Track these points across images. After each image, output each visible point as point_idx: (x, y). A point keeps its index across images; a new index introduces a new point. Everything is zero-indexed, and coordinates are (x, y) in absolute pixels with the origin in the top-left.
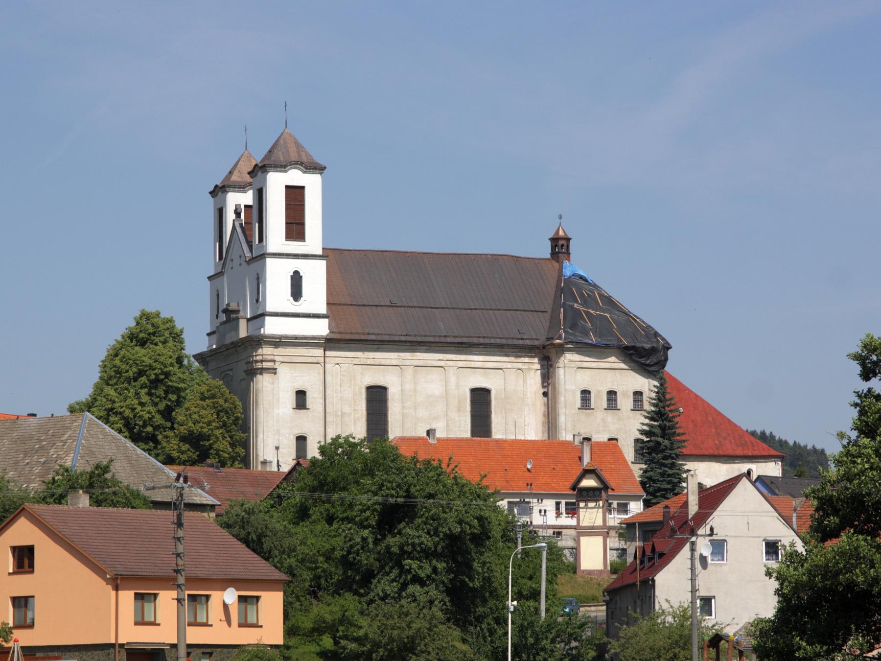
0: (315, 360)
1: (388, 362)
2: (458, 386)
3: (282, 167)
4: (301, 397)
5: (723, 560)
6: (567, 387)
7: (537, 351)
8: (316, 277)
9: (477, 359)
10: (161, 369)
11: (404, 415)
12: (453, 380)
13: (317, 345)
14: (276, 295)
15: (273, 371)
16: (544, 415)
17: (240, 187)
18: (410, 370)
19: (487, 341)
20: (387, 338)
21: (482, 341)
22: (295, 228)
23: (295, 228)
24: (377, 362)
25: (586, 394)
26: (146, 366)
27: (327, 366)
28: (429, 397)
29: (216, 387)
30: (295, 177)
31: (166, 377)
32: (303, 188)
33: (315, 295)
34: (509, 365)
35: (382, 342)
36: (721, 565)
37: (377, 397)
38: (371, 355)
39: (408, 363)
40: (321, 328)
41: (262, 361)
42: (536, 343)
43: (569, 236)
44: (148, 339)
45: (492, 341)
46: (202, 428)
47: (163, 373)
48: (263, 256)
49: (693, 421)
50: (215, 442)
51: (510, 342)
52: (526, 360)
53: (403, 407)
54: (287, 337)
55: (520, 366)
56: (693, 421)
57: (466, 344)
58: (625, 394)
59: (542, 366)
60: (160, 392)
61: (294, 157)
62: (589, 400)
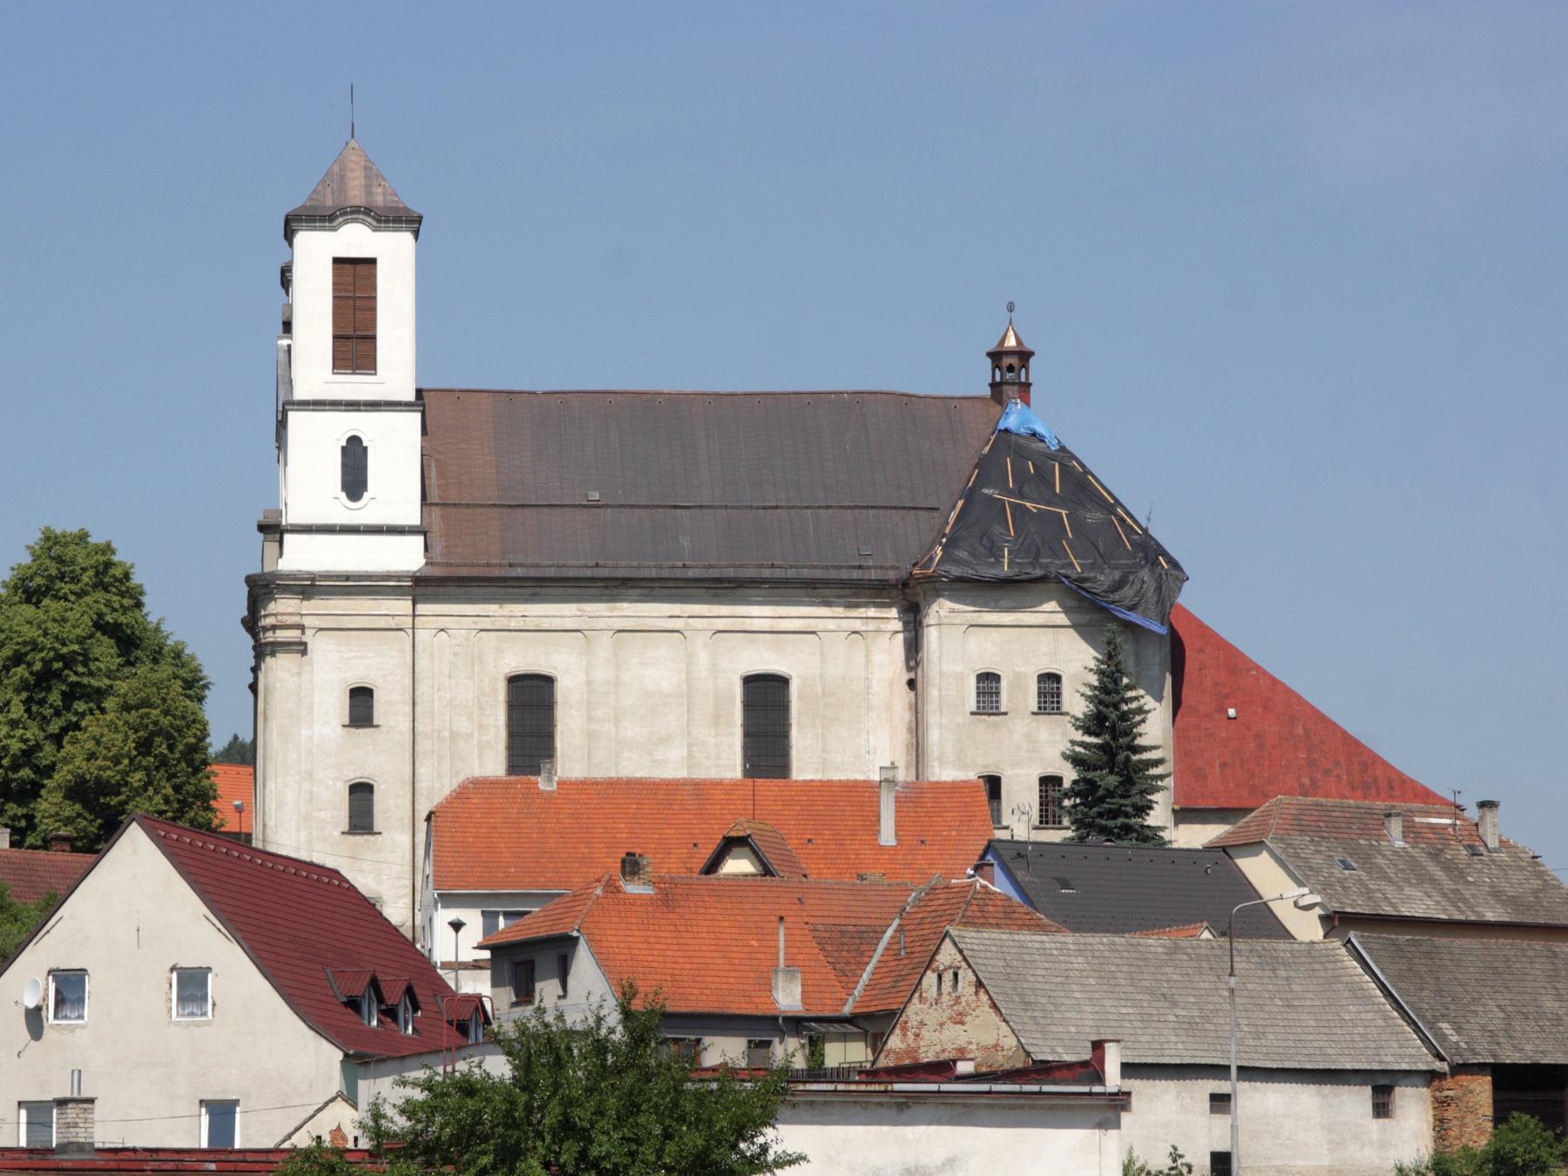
0: (392, 623)
1: (545, 624)
3: (324, 218)
4: (361, 704)
5: (81, 1017)
6: (944, 668)
7: (894, 592)
8: (396, 448)
9: (759, 614)
10: (53, 648)
11: (591, 737)
12: (703, 658)
13: (397, 592)
14: (310, 485)
15: (302, 648)
16: (909, 730)
17: (323, 219)
18: (606, 638)
19: (778, 573)
20: (551, 573)
22: (355, 345)
23: (355, 345)
24: (520, 624)
25: (988, 682)
26: (25, 643)
28: (649, 693)
29: (154, 684)
30: (355, 239)
31: (67, 666)
32: (372, 262)
33: (396, 487)
34: (832, 624)
36: (74, 1028)
37: (531, 700)
39: (601, 624)
40: (408, 556)
41: (274, 628)
42: (891, 575)
43: (1029, 345)
44: (48, 588)
45: (791, 573)
46: (100, 768)
47: (60, 657)
48: (287, 406)
49: (1257, 736)
50: (129, 799)
51: (833, 574)
52: (872, 612)
53: (590, 719)
56: (1257, 736)
57: (730, 580)
59: (906, 624)
60: (55, 698)
61: (356, 196)
62: (998, 694)
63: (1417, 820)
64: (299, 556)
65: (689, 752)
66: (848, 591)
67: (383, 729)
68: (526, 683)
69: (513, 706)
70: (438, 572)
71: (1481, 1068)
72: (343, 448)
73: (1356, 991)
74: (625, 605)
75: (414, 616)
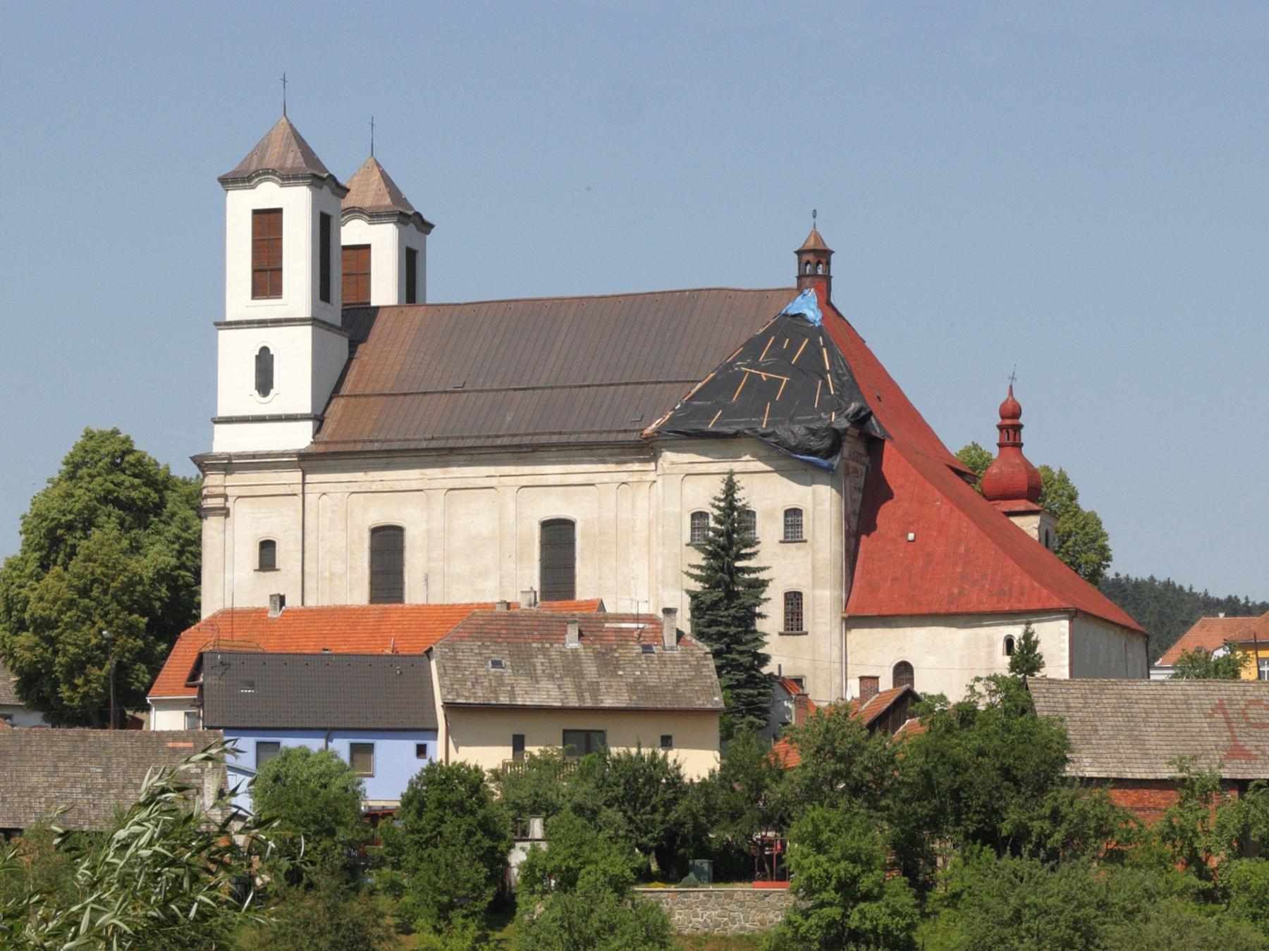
0: (288, 490)
2: (518, 517)
4: (267, 548)
9: (552, 472)
12: (511, 508)
14: (235, 391)
15: (225, 512)
17: (243, 181)
19: (564, 439)
21: (555, 439)
22: (267, 279)
23: (267, 279)
27: (308, 497)
30: (268, 194)
33: (296, 386)
34: (606, 478)
35: (390, 453)
37: (387, 545)
39: (436, 484)
40: (300, 437)
45: (573, 439)
52: (636, 466)
53: (429, 559)
54: (240, 456)
55: (624, 477)
58: (770, 515)
63: (607, 625)
64: (227, 441)
65: (501, 582)
66: (616, 451)
67: (282, 572)
68: (385, 533)
70: (321, 449)
72: (257, 357)
74: (455, 469)
75: (304, 484)
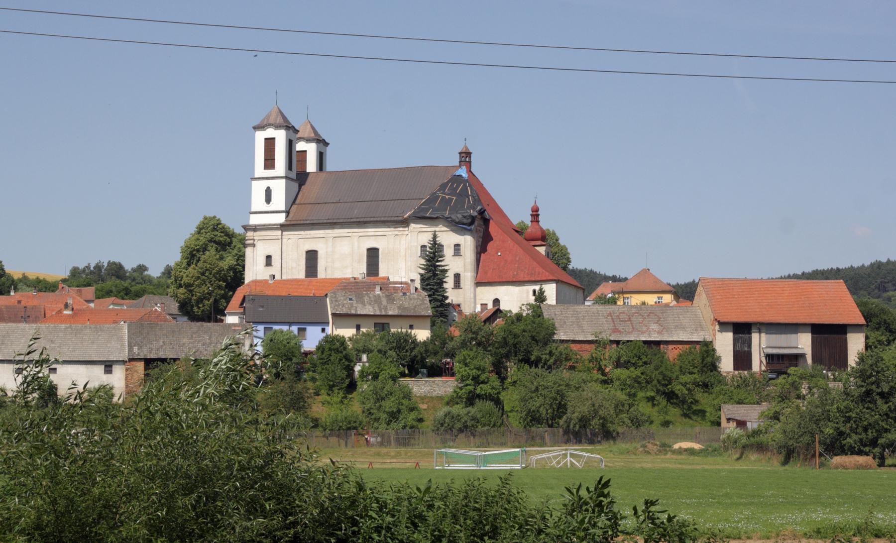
3: (260, 127)
4: (269, 258)
9: (371, 231)
13: (276, 229)
14: (258, 201)
15: (254, 245)
22: (269, 163)
23: (269, 163)
30: (270, 133)
32: (274, 139)
33: (279, 201)
35: (313, 224)
37: (312, 257)
38: (308, 232)
40: (281, 219)
51: (389, 219)
55: (397, 233)
64: (254, 220)
69: (307, 260)
71: (140, 359)
73: (121, 339)
